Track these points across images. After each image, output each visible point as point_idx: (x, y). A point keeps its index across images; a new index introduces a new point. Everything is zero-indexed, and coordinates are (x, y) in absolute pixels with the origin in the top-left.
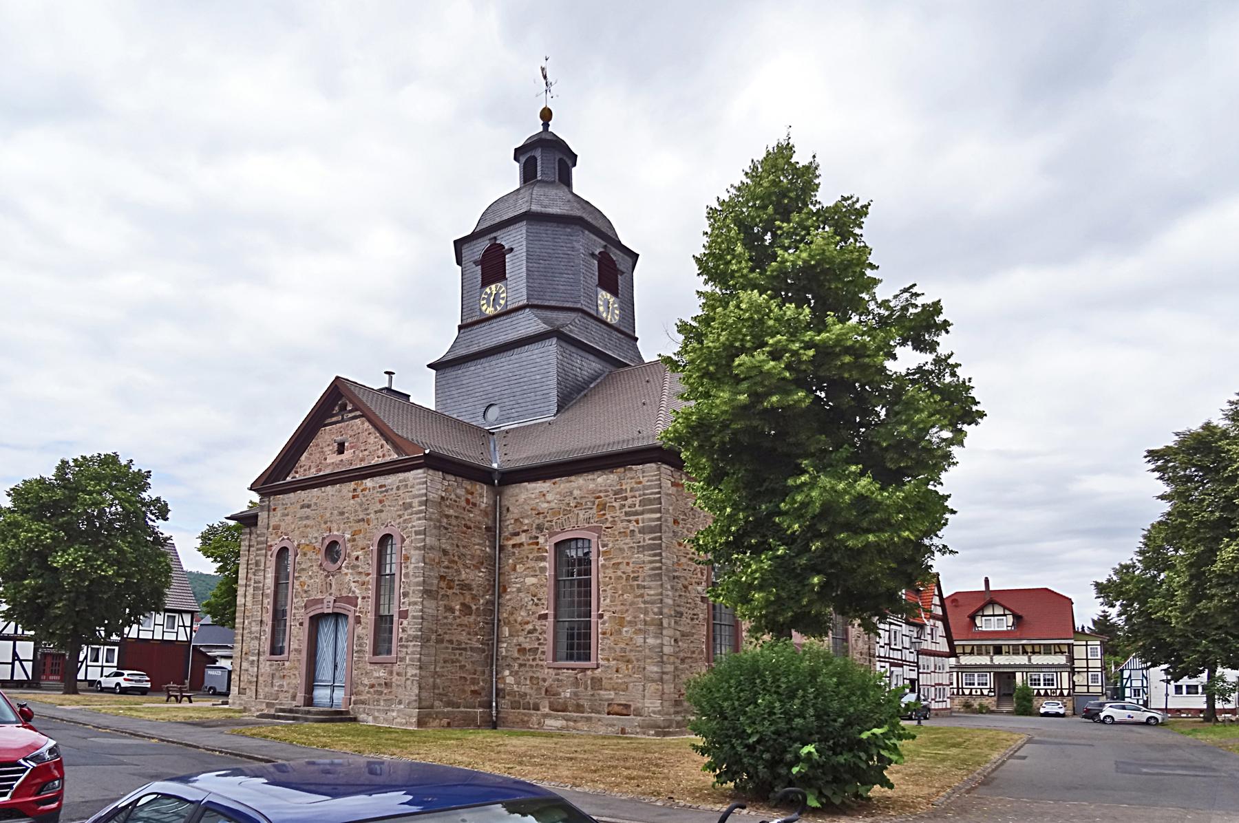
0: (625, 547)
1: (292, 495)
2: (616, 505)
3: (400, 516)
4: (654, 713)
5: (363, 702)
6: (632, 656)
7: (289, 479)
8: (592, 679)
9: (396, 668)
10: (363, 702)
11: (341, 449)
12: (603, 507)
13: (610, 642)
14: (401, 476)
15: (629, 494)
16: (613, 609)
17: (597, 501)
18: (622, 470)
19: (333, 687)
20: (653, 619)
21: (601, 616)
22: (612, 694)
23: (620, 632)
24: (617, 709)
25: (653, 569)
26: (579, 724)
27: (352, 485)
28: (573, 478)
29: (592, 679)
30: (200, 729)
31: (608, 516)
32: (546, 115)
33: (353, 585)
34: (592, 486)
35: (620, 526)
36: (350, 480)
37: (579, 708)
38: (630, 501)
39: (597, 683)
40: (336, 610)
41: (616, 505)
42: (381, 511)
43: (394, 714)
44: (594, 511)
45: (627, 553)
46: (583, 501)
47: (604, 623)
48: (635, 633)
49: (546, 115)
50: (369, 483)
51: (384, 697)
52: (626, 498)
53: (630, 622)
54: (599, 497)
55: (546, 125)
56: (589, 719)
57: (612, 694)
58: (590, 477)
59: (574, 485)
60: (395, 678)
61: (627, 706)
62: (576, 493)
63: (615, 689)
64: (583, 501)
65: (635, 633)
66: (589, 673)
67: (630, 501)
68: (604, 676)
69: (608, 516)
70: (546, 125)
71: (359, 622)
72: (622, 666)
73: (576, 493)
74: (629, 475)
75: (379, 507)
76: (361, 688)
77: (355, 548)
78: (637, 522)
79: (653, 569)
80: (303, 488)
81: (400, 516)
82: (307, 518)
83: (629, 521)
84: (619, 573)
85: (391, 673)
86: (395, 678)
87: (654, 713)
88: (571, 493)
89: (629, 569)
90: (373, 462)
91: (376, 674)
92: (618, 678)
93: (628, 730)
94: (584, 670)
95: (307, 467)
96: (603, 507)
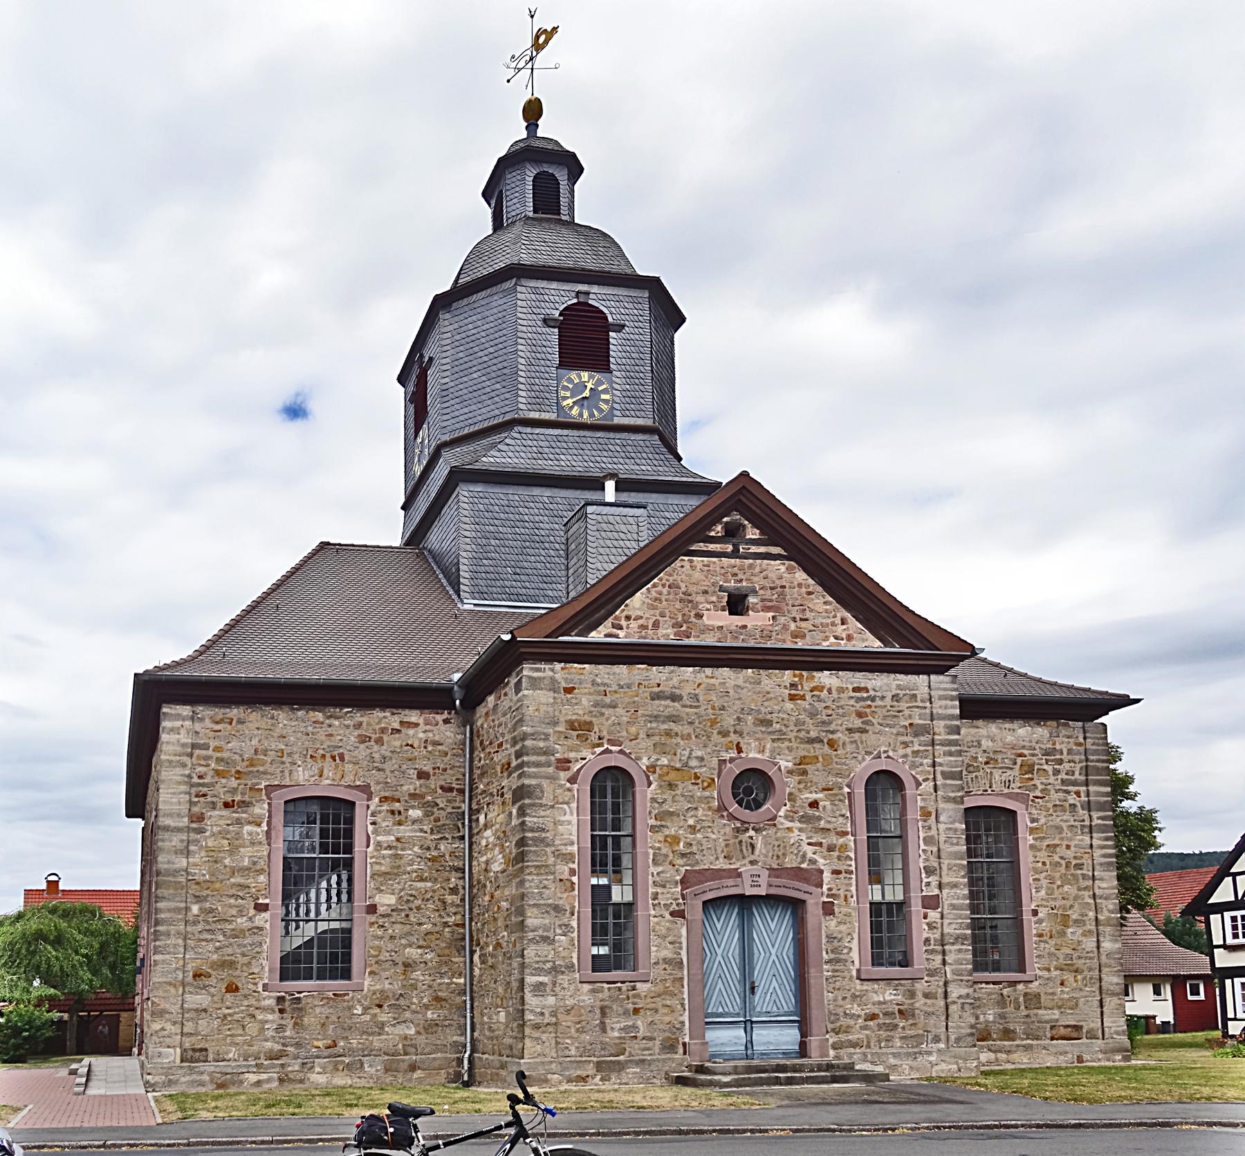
0: (1064, 825)
1: (622, 669)
2: (1049, 768)
3: (906, 745)
4: (1118, 1033)
5: (854, 1045)
6: (1079, 963)
7: (596, 636)
8: (1026, 994)
9: (920, 987)
10: (854, 1045)
11: (736, 604)
12: (1029, 768)
13: (1050, 946)
14: (903, 679)
15: (1065, 757)
16: (1053, 904)
17: (1019, 760)
18: (1054, 724)
19: (748, 1025)
20: (1109, 919)
21: (1035, 913)
22: (1056, 1014)
23: (1063, 934)
24: (1063, 1031)
25: (1104, 856)
26: (1015, 1056)
27: (788, 676)
28: (980, 723)
29: (1026, 994)
30: (839, 1107)
31: (1036, 782)
32: (533, 111)
33: (809, 850)
34: (1009, 739)
35: (1055, 797)
36: (783, 666)
37: (1008, 1034)
38: (1067, 766)
39: (1033, 1000)
40: (773, 891)
41: (1049, 768)
42: (863, 731)
43: (933, 1058)
44: (1016, 771)
45: (1067, 833)
46: (999, 757)
47: (1040, 922)
48: (1084, 935)
49: (533, 111)
50: (826, 678)
51: (898, 1033)
52: (1060, 762)
53: (1076, 921)
54: (1020, 755)
55: (532, 125)
56: (1027, 1048)
57: (1056, 1014)
58: (1007, 726)
59: (983, 732)
60: (920, 1002)
61: (1078, 1028)
62: (986, 744)
63: (1060, 1007)
64: (999, 757)
65: (1084, 935)
66: (1020, 987)
67: (1067, 766)
68: (1042, 991)
69: (1036, 782)
70: (532, 125)
71: (832, 913)
72: (1069, 977)
73: (986, 744)
74: (1064, 732)
75: (858, 723)
76: (844, 1022)
77: (806, 786)
78: (1078, 794)
79: (1104, 856)
80: (652, 662)
81: (906, 745)
82: (674, 719)
83: (1068, 792)
84: (1056, 858)
85: (912, 994)
86: (920, 1002)
87: (1118, 1033)
88: (979, 745)
89: (1069, 854)
90: (825, 645)
91: (876, 998)
92: (1063, 993)
93: (1085, 1057)
94: (1013, 984)
95: (639, 617)
96: (1029, 768)
